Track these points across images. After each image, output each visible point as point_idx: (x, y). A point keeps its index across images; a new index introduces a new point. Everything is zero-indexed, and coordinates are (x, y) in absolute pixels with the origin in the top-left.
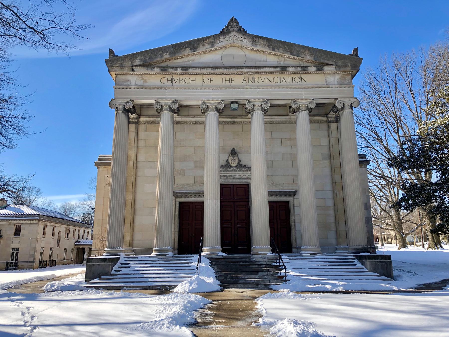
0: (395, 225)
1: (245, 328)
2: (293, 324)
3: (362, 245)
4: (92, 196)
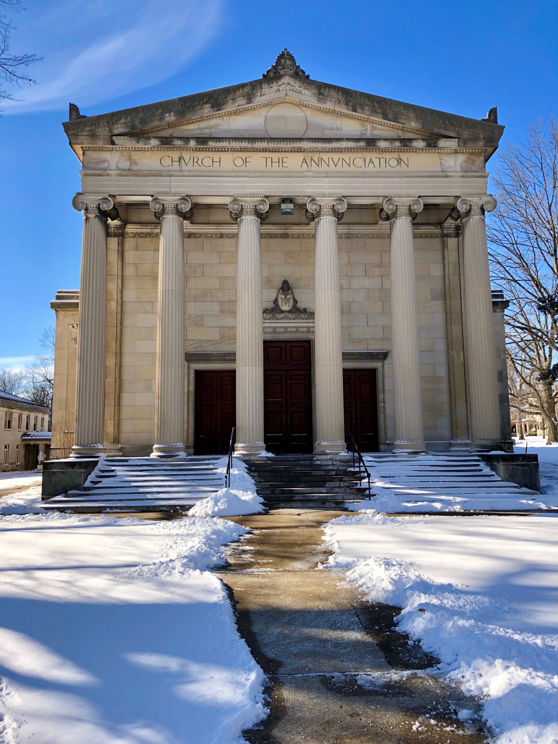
0: (544, 405)
1: (306, 573)
2: (383, 565)
3: (493, 438)
4: (47, 359)
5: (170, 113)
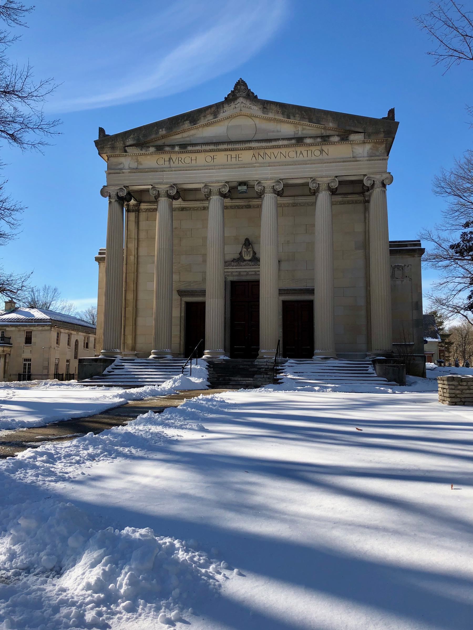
5: (162, 129)
